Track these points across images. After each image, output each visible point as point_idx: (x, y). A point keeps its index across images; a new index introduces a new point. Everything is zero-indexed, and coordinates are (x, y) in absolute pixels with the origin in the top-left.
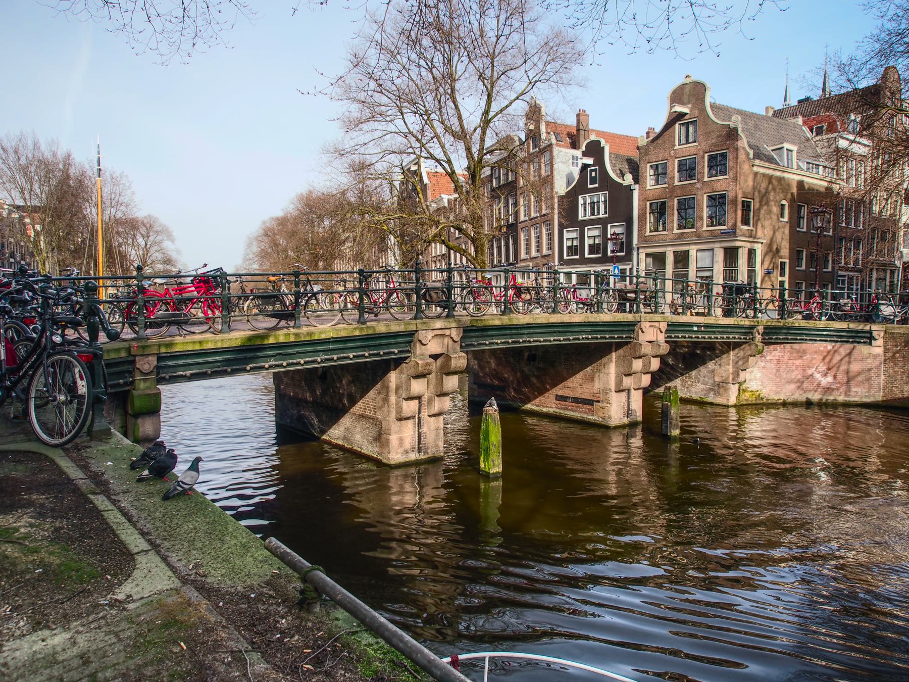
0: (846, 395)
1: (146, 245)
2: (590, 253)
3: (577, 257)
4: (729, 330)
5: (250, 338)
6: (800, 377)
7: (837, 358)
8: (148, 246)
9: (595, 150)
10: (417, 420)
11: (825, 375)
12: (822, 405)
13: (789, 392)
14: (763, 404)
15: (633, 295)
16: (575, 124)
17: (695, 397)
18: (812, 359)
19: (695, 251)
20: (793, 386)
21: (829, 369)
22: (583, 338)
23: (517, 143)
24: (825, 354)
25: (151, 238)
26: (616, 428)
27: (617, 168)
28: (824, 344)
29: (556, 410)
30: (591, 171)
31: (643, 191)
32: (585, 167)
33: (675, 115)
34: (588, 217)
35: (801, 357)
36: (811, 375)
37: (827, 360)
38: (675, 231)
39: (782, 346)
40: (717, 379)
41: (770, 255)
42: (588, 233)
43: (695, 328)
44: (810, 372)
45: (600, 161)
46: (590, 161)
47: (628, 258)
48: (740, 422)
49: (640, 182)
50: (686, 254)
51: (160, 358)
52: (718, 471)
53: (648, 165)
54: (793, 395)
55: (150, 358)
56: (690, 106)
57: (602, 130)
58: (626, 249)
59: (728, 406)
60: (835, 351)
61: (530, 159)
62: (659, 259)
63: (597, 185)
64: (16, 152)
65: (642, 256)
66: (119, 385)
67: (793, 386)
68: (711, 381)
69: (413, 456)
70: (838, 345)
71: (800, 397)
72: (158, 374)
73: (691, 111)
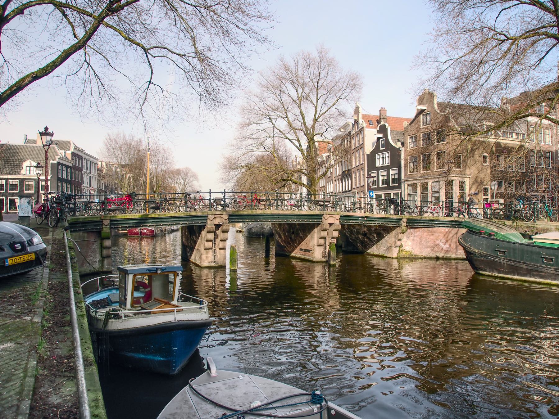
0: (456, 255)
1: (184, 183)
2: (383, 184)
3: (376, 187)
4: (383, 220)
5: (142, 216)
6: (432, 245)
7: (451, 235)
8: (186, 184)
9: (383, 130)
10: (213, 251)
11: (445, 244)
12: (443, 259)
13: (427, 252)
14: (414, 258)
15: (322, 203)
16: (379, 115)
17: (381, 254)
18: (439, 236)
19: (431, 182)
20: (429, 249)
21: (447, 241)
22: (306, 221)
23: (351, 126)
24: (445, 233)
25: (187, 180)
26: (318, 262)
27: (396, 139)
28: (444, 228)
29: (300, 256)
30: (382, 141)
31: (406, 150)
32: (379, 139)
33: (420, 110)
34: (381, 165)
35: (433, 235)
36: (438, 244)
37: (446, 236)
38: (422, 172)
39: (422, 229)
40: (389, 245)
41: (477, 184)
42: (381, 173)
43: (360, 219)
44: (437, 242)
45: (386, 136)
46: (381, 135)
47: (399, 187)
48: (400, 267)
49: (405, 146)
50: (427, 184)
51: (111, 221)
52: (418, 298)
53: (408, 137)
54: (429, 254)
55: (107, 220)
56: (427, 105)
57: (399, 117)
58: (398, 181)
59: (392, 258)
60: (450, 232)
61: (357, 134)
62: (414, 186)
63: (384, 148)
64: (115, 141)
65: (406, 186)
66: (97, 229)
67: (429, 249)
68: (386, 246)
69: (212, 264)
70: (451, 229)
71: (434, 255)
72: (110, 226)
73: (427, 108)
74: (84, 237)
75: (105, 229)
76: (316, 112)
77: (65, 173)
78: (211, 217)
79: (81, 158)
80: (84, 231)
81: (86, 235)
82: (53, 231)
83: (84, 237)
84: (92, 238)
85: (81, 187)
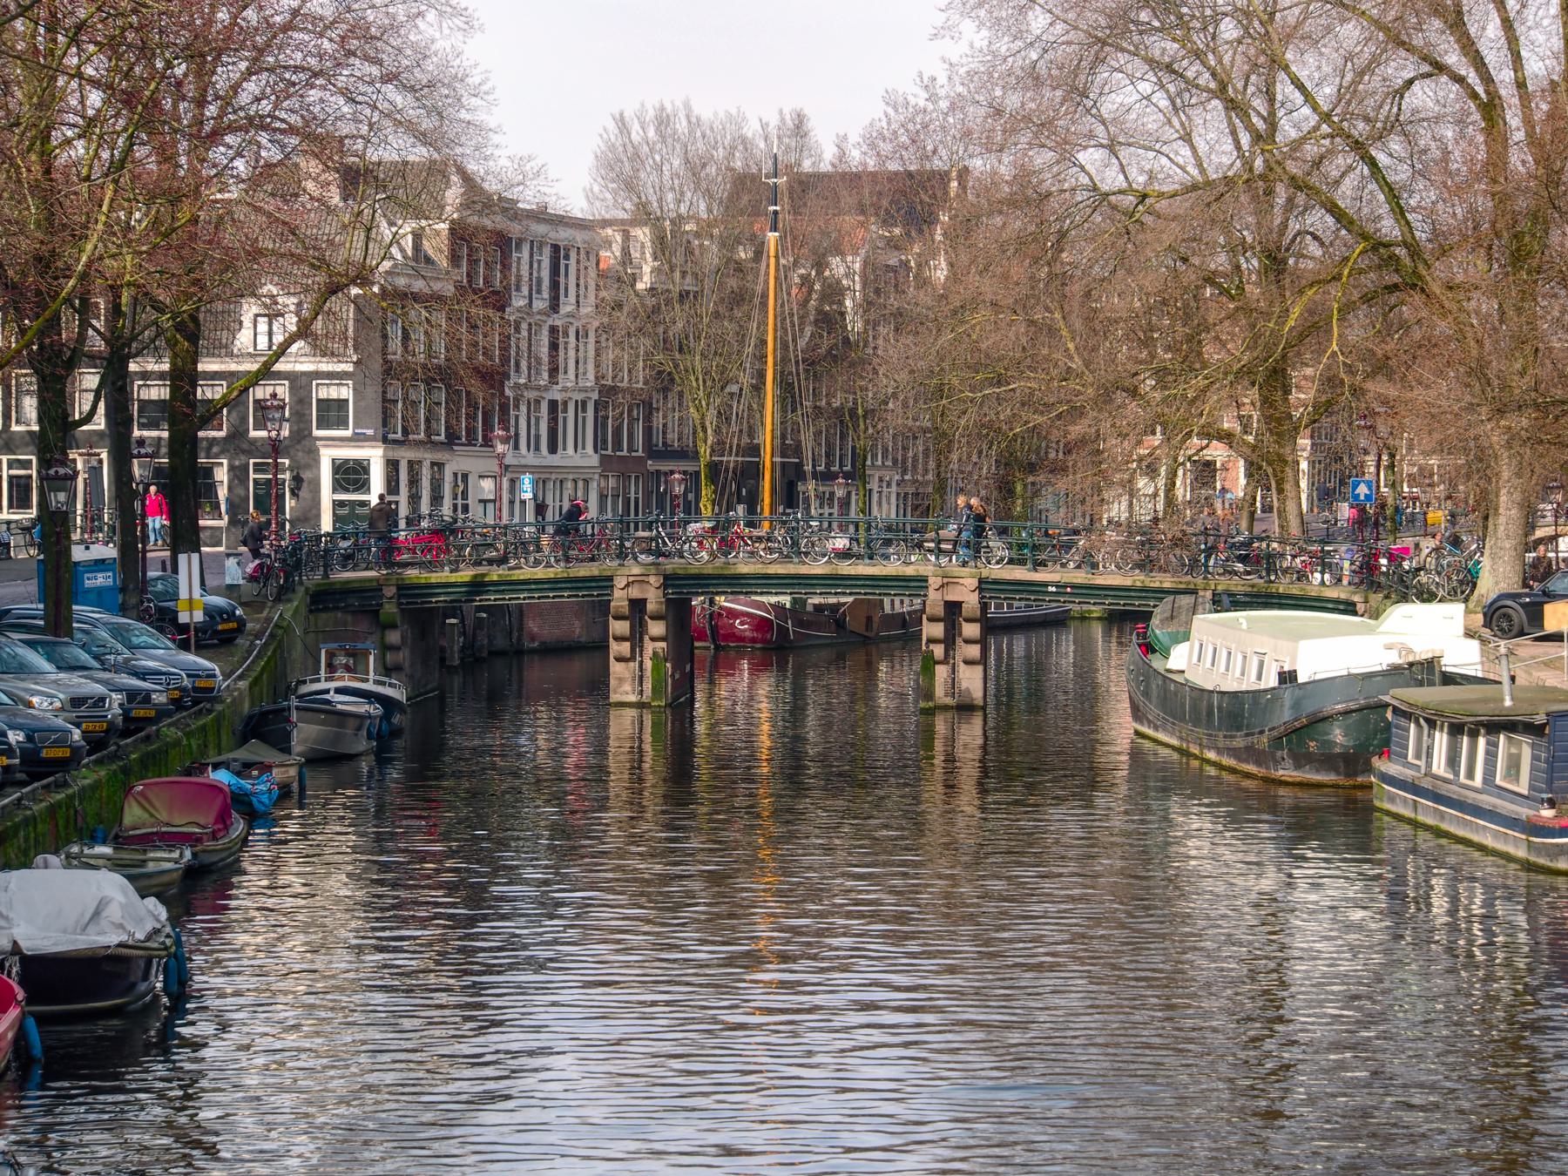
74: (345, 625)
75: (387, 606)
76: (1460, 80)
77: (418, 335)
78: (620, 582)
79: (504, 243)
80: (345, 610)
81: (349, 618)
82: (271, 608)
83: (345, 625)
84: (363, 626)
85: (502, 393)
